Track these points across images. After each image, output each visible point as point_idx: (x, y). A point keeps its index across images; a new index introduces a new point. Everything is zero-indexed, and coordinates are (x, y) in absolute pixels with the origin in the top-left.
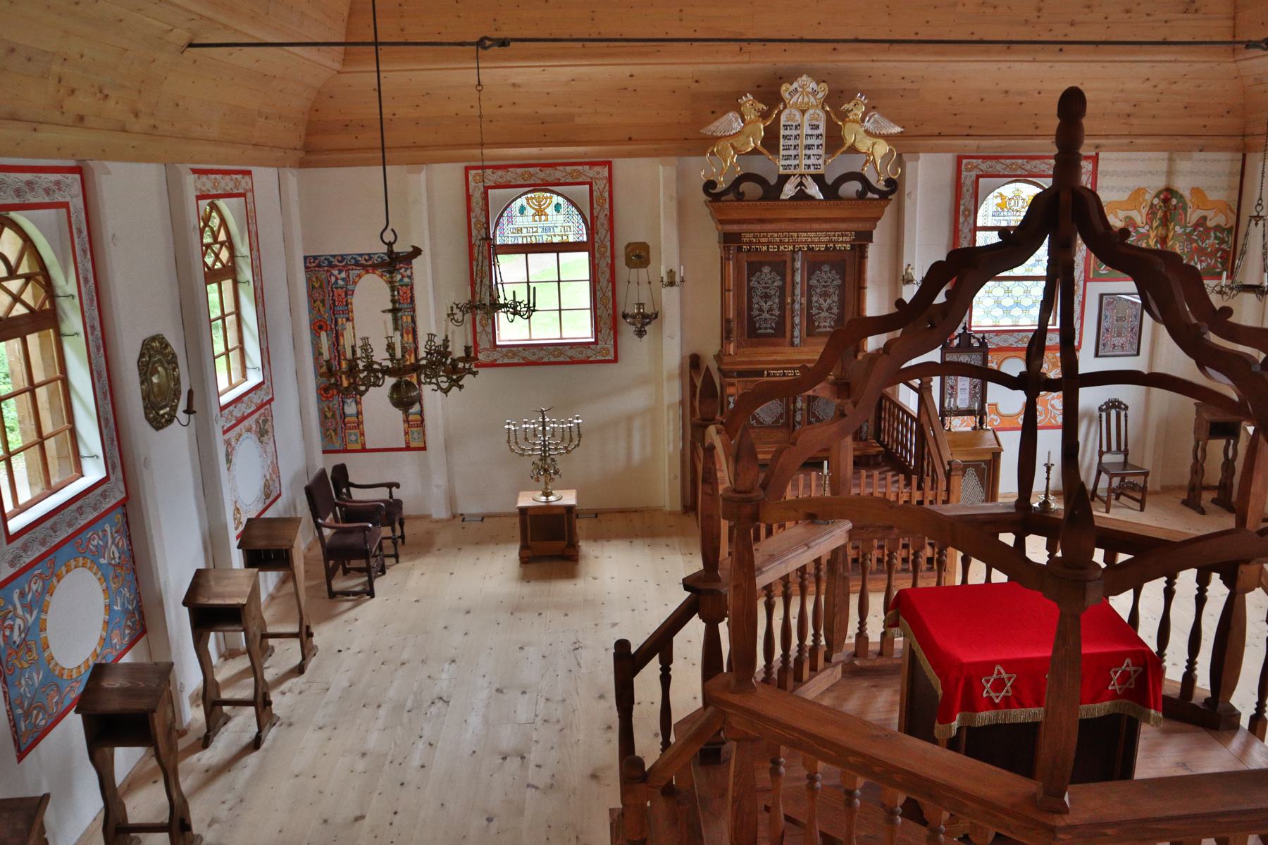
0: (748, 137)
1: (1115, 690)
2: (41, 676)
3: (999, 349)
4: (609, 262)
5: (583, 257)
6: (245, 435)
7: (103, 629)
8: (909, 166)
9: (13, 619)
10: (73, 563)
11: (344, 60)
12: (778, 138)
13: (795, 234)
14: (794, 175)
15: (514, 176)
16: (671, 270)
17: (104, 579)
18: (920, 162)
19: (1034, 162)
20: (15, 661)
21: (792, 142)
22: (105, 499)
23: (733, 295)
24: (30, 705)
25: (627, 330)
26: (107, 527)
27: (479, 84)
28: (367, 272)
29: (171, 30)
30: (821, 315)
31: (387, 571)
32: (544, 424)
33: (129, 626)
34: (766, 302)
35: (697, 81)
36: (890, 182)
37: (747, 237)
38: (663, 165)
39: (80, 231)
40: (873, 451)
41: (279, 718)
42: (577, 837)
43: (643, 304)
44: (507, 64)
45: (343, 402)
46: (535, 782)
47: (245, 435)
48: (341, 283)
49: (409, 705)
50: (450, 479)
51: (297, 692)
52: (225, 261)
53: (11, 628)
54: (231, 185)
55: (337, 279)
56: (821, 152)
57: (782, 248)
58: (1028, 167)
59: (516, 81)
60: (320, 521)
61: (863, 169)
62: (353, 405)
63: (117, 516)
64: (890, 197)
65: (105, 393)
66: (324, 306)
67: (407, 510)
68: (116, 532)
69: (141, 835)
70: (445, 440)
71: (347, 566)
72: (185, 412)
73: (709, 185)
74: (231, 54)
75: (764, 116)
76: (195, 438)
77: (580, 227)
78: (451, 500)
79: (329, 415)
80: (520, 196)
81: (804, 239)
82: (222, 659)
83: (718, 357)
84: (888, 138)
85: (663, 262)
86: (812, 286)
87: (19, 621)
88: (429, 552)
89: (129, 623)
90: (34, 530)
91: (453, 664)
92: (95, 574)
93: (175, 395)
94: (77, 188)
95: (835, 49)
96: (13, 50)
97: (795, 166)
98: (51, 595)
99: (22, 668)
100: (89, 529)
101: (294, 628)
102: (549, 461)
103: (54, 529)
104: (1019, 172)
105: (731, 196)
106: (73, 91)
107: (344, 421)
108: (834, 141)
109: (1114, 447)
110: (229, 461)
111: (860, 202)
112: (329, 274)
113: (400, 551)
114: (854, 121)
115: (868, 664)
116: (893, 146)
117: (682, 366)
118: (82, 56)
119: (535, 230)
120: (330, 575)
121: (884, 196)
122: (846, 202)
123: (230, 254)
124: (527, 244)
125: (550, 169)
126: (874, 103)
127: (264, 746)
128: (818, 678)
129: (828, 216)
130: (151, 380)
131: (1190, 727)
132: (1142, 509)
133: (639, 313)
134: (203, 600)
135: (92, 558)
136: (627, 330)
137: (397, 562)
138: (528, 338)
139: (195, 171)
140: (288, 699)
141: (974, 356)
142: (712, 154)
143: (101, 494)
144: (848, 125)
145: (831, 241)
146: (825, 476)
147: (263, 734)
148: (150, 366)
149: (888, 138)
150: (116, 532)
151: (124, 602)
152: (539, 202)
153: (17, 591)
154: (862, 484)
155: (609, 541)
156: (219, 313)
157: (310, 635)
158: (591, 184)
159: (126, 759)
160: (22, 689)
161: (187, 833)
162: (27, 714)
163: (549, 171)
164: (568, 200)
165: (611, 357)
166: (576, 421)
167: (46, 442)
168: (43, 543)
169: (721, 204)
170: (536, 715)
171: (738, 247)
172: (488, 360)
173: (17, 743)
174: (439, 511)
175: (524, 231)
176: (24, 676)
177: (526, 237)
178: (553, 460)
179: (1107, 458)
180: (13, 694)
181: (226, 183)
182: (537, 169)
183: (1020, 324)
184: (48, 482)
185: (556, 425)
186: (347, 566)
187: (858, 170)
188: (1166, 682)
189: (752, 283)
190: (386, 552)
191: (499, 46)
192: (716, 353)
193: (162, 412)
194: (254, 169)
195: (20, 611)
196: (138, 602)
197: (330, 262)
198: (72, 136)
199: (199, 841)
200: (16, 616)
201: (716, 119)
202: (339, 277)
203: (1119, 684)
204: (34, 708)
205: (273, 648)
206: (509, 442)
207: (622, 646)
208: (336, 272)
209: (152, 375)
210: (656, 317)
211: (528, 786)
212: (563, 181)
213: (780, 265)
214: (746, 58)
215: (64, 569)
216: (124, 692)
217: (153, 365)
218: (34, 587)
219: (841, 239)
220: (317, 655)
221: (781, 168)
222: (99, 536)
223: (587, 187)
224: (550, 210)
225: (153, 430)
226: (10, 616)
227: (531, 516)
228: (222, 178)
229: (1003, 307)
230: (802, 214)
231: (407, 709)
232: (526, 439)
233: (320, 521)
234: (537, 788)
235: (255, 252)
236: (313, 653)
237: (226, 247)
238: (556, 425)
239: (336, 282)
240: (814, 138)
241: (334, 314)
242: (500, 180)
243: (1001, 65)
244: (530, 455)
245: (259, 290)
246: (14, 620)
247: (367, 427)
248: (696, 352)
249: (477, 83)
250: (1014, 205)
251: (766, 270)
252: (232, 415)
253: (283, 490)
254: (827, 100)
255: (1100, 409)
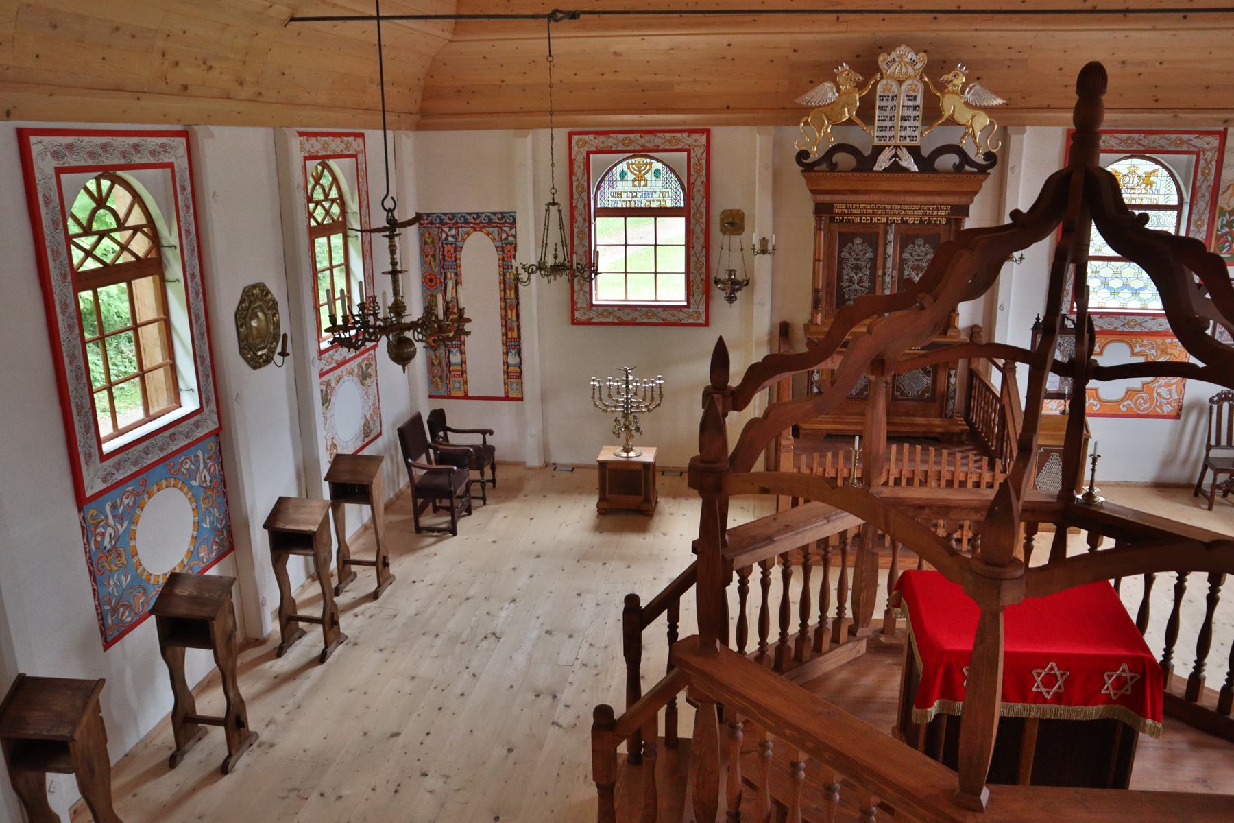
0: (843, 107)
1: (1110, 694)
2: (129, 579)
3: (1104, 332)
4: (704, 228)
5: (681, 222)
6: (346, 378)
7: (191, 543)
8: (1014, 139)
9: (105, 527)
10: (164, 483)
11: (455, 29)
12: (874, 108)
13: (888, 207)
14: (889, 147)
15: (615, 142)
16: (764, 238)
17: (194, 499)
18: (1025, 135)
19: (1152, 137)
20: (105, 564)
21: (888, 113)
22: (197, 428)
23: (823, 264)
24: (117, 603)
25: (719, 295)
26: (200, 454)
27: (550, 55)
28: (475, 230)
29: (271, 6)
30: (851, 288)
31: (474, 512)
32: (627, 383)
33: (217, 543)
34: (856, 274)
35: (795, 51)
36: (989, 156)
37: (839, 208)
38: (759, 134)
39: (183, 189)
40: (957, 429)
41: (347, 637)
42: (586, 776)
43: (734, 271)
44: (607, 33)
45: (449, 351)
46: (560, 721)
47: (346, 378)
48: (450, 239)
49: (464, 637)
50: (545, 430)
51: (368, 616)
52: (320, 220)
53: (103, 535)
54: (342, 146)
55: (447, 235)
56: (918, 123)
57: (875, 220)
58: (1145, 142)
59: (617, 50)
60: (410, 460)
61: (961, 142)
62: (458, 354)
63: (211, 444)
64: (988, 171)
65: (202, 335)
66: (435, 260)
67: (498, 455)
68: (208, 458)
69: (209, 727)
70: (542, 391)
71: (438, 504)
72: (279, 354)
73: (802, 155)
74: (335, 26)
75: (860, 86)
76: (293, 380)
77: (678, 193)
78: (545, 449)
79: (436, 363)
80: (621, 162)
81: (897, 212)
82: (309, 580)
83: (807, 327)
84: (989, 110)
85: (757, 230)
86: (905, 260)
87: (110, 530)
88: (516, 497)
89: (217, 540)
90: (127, 452)
91: (512, 604)
92: (186, 494)
93: (274, 337)
94: (182, 150)
95: (936, 18)
96: (117, 29)
97: (890, 138)
98: (142, 510)
99: (111, 570)
100: (180, 454)
101: (372, 558)
102: (631, 418)
103: (146, 452)
104: (1134, 148)
105: (824, 166)
106: (177, 64)
107: (449, 369)
108: (931, 112)
109: (1224, 442)
110: (326, 400)
111: (957, 175)
112: (440, 230)
113: (487, 494)
114: (954, 93)
115: (894, 641)
116: (992, 117)
117: (771, 334)
118: (185, 32)
119: (634, 194)
120: (418, 512)
121: (983, 170)
122: (942, 176)
123: (341, 210)
124: (626, 208)
125: (650, 135)
126: (978, 74)
127: (329, 661)
128: (838, 650)
129: (921, 189)
130: (250, 324)
131: (1223, 742)
132: (1210, 509)
133: (730, 279)
134: (281, 525)
135: (183, 480)
136: (719, 295)
137: (485, 504)
138: (624, 298)
139: (301, 134)
140: (359, 621)
141: (1067, 338)
142: (806, 123)
143: (194, 424)
144: (947, 97)
145: (925, 215)
146: (856, 452)
147: (328, 651)
148: (250, 311)
149: (989, 110)
150: (208, 458)
151: (213, 521)
152: (639, 168)
153: (110, 503)
154: (930, 461)
155: (687, 499)
156: (326, 264)
157: (386, 565)
158: (689, 151)
159: (199, 662)
160: (111, 589)
161: (242, 729)
162: (114, 610)
163: (648, 137)
164: (667, 166)
165: (702, 321)
166: (658, 381)
167: (146, 375)
168: (135, 463)
169: (813, 174)
170: (577, 659)
171: (830, 217)
172: (584, 318)
173: (103, 633)
174: (533, 459)
175: (624, 195)
176: (113, 577)
177: (625, 201)
178: (635, 417)
179: (1214, 453)
180: (102, 591)
181: (337, 145)
182: (638, 136)
183: (1149, 307)
184: (146, 410)
185: (638, 384)
186: (438, 504)
187: (956, 143)
188: (1205, 691)
189: (843, 254)
190: (473, 494)
191: (570, 18)
192: (806, 322)
193: (260, 353)
194: (366, 132)
195: (111, 521)
196: (227, 522)
197: (441, 220)
198: (178, 106)
199: (254, 738)
200: (107, 525)
201: (813, 88)
202: (449, 233)
203: (1113, 689)
204: (121, 606)
205: (355, 574)
206: (593, 397)
207: (631, 601)
208: (446, 229)
209: (251, 319)
210: (747, 284)
211: (553, 723)
212: (661, 147)
213: (873, 238)
214: (842, 28)
215: (155, 488)
216: (193, 600)
217: (253, 311)
218: (126, 501)
219: (936, 213)
220: (394, 583)
221: (876, 139)
222: (191, 461)
223: (686, 153)
224: (649, 176)
225: (252, 370)
226: (102, 523)
227: (609, 470)
228: (333, 140)
229: (1109, 288)
230: (896, 186)
231: (461, 641)
232: (610, 396)
233: (410, 460)
234: (561, 726)
235: (364, 208)
236: (389, 581)
237: (337, 203)
238: (638, 384)
239: (446, 239)
240: (911, 109)
241: (444, 269)
242: (602, 146)
243: (1117, 34)
244: (613, 411)
245: (367, 244)
246: (106, 530)
247: (470, 376)
248: (786, 320)
249: (548, 54)
250: (1129, 182)
251: (858, 241)
252: (332, 359)
253: (384, 433)
254: (927, 70)
255: (1211, 400)
